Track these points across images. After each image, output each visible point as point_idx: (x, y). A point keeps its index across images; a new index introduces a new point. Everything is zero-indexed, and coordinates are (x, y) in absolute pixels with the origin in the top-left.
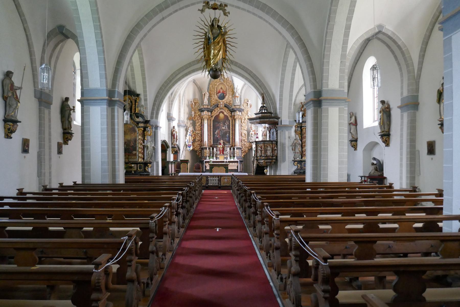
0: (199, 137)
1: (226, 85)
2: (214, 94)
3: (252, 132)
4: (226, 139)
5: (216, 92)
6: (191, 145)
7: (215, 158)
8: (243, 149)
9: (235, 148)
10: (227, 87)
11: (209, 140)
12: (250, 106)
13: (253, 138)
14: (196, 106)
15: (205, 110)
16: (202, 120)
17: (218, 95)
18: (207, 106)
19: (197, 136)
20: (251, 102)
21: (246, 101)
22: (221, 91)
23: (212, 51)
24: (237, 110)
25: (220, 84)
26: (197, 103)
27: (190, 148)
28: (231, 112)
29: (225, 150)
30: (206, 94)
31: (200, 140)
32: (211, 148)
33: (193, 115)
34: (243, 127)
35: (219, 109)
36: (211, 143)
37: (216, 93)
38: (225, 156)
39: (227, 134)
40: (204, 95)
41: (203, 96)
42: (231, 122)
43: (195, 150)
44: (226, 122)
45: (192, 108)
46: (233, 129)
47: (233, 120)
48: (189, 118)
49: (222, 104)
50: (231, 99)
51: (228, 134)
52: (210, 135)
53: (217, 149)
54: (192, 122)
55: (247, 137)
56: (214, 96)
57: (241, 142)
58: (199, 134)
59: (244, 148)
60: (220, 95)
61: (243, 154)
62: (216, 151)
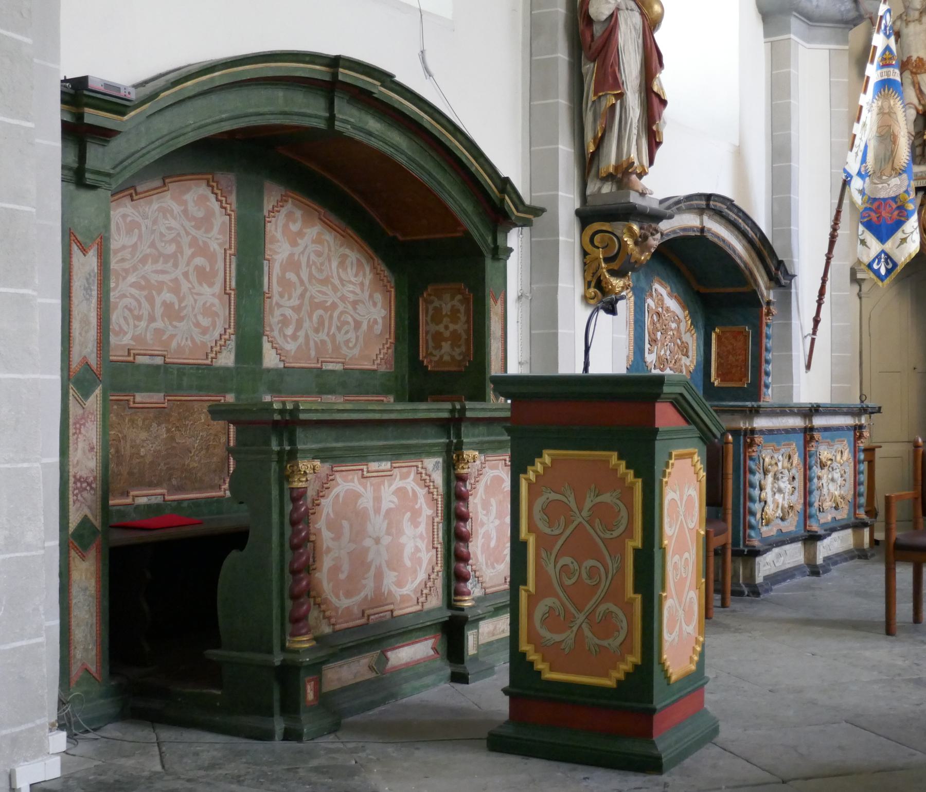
6: (902, 208)
27: (889, 246)
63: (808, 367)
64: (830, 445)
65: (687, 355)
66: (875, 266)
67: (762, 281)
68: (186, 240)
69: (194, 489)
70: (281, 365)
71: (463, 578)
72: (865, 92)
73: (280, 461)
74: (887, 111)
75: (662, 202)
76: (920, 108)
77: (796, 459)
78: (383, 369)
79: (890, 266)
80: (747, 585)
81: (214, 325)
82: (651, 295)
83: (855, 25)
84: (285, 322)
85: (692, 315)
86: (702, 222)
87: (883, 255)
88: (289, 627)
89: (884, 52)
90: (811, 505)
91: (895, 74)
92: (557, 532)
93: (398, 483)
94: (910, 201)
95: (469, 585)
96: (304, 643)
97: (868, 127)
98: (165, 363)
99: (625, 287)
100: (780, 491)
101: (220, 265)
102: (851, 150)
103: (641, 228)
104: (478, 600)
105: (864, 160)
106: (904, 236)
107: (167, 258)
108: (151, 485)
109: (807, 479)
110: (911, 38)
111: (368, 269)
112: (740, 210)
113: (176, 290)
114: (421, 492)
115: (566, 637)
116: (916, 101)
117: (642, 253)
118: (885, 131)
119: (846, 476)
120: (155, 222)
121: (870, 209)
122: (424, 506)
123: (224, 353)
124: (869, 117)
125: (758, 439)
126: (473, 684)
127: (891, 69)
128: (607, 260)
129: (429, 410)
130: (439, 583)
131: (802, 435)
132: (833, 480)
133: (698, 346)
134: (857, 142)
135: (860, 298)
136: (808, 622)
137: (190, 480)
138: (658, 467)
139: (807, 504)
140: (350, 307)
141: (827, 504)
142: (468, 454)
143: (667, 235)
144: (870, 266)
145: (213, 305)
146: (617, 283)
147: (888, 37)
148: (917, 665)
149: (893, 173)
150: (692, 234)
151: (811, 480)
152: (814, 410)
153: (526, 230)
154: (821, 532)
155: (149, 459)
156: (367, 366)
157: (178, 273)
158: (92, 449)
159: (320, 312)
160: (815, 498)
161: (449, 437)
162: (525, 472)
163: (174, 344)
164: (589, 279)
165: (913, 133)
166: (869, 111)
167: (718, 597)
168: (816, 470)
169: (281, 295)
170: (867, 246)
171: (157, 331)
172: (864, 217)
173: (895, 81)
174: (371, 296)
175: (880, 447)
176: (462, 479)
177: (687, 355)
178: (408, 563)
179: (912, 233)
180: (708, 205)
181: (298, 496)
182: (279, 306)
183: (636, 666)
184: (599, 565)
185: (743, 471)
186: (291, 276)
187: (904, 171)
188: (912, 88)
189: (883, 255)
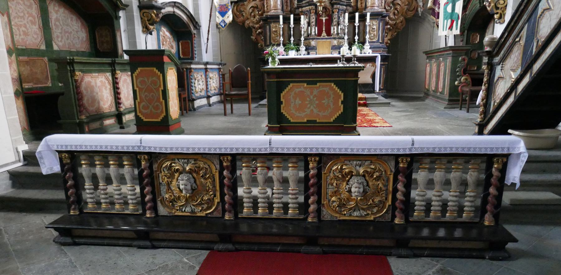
7: (304, 48)
8: (390, 18)
9: (368, 14)
32: (292, 16)
38: (335, 42)
59: (392, 16)
62: (306, 25)
63: (206, 52)
64: (212, 73)
65: (173, 48)
66: (221, 24)
67: (192, 28)
68: (26, 12)
69: (41, 84)
70: (59, 49)
71: (120, 104)
73: (71, 73)
75: (162, 3)
77: (203, 76)
78: (88, 51)
79: (225, 24)
80: (192, 108)
81: (38, 37)
82: (161, 31)
84: (58, 37)
85: (173, 37)
86: (174, 10)
88: (79, 114)
90: (208, 88)
92: (143, 87)
93: (100, 79)
95: (122, 105)
96: (83, 117)
98: (26, 48)
99: (154, 28)
100: (199, 84)
101: (37, 20)
103: (156, 12)
104: (125, 110)
107: (22, 17)
108: (28, 82)
109: (207, 82)
111: (79, 21)
112: (184, 6)
113: (25, 27)
114: (107, 82)
115: (148, 111)
117: (157, 19)
119: (217, 81)
120: (16, 6)
122: (108, 86)
123: (42, 45)
125: (193, 70)
126: (127, 129)
128: (148, 20)
129: (106, 60)
130: (114, 105)
131: (204, 70)
132: (213, 82)
133: (176, 46)
135: (219, 33)
136: (207, 115)
137: (38, 81)
138: (165, 71)
139: (207, 88)
140: (76, 32)
141: (213, 89)
142: (118, 72)
143: (164, 13)
144: (220, 24)
145: (36, 31)
146: (151, 27)
150: (171, 13)
151: (207, 82)
152: (207, 63)
153: (124, 11)
154: (211, 95)
155: (26, 75)
156: (83, 50)
157: (25, 22)
158: (15, 71)
159: (68, 34)
160: (209, 86)
161: (112, 67)
162: (134, 73)
163: (28, 43)
164: (143, 26)
167: (185, 111)
168: (209, 80)
169: (56, 29)
171: (22, 39)
174: (81, 30)
176: (117, 78)
177: (173, 48)
178: (106, 100)
180: (175, 5)
181: (76, 81)
182: (56, 32)
183: (164, 116)
184: (154, 94)
185: (189, 79)
186: (57, 23)
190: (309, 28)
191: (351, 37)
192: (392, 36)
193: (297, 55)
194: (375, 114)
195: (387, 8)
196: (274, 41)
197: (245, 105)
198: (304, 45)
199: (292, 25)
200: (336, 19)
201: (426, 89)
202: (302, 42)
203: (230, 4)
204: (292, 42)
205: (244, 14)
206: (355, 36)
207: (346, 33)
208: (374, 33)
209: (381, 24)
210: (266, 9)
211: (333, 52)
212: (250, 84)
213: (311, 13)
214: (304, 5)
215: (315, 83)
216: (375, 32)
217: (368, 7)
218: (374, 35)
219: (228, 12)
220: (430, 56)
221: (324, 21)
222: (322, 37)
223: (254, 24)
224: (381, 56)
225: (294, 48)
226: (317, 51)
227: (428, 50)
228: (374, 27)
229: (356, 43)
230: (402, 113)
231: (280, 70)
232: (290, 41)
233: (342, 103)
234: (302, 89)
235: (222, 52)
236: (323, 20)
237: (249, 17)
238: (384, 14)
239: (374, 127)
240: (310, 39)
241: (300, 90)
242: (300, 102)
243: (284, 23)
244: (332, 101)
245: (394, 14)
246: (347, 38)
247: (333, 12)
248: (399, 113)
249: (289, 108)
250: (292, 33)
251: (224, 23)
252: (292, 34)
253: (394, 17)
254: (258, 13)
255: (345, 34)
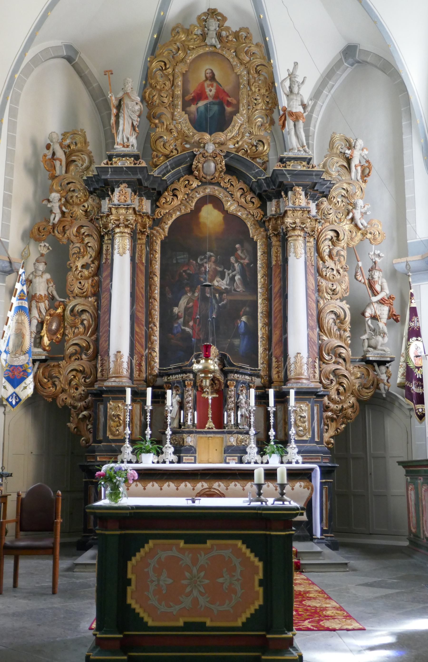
0: (81, 329)
1: (235, 62)
2: (173, 106)
3: (376, 305)
4: (237, 342)
5: (184, 96)
6: (25, 371)
7: (172, 449)
8: (330, 399)
9: (292, 393)
10: (240, 70)
11: (138, 347)
12: (359, 168)
13: (386, 339)
14: (72, 167)
15: (118, 183)
16: (102, 237)
17: (193, 108)
18: (128, 163)
19: (74, 326)
20: (366, 152)
21: (340, 145)
22: (207, 90)
23: (206, 482)
24: (298, 185)
25: (200, 56)
26: (79, 151)
27: (18, 390)
28: (260, 196)
29: (232, 405)
30: (127, 101)
31: (88, 348)
32: (149, 391)
33: (57, 210)
34: (325, 278)
35: (195, 185)
36: (149, 364)
37: (180, 103)
38: (233, 440)
39: (239, 317)
40: (119, 107)
41: (114, 111)
42: (259, 254)
43: (60, 403)
44: (233, 252)
45: (53, 177)
46: (276, 289)
47: (274, 240)
48: (36, 231)
49: (214, 156)
50: (262, 133)
51: (244, 319)
52: (149, 322)
53: (182, 396)
54: (51, 252)
55: (348, 334)
56: (169, 116)
57: (321, 358)
58: (85, 316)
59: (334, 395)
60: (202, 109)
61: (333, 426)
62: (176, 407)
66: (10, 400)
72: (10, 310)
74: (20, 322)
76: (40, 319)
83: (9, 274)
87: (14, 394)
89: (20, 293)
91: (26, 304)
94: (29, 368)
97: (11, 328)
102: (2, 339)
105: (7, 345)
106: (26, 385)
110: (37, 284)
116: (37, 316)
118: (19, 331)
121: (9, 371)
124: (12, 323)
127: (24, 301)
134: (5, 335)
135: (5, 414)
144: (7, 400)
147: (23, 285)
148: (9, 607)
149: (22, 353)
165: (35, 332)
166: (12, 320)
170: (6, 389)
172: (6, 374)
173: (25, 307)
175: (10, 495)
179: (29, 384)
187: (27, 353)
188: (36, 309)
189: (14, 394)
190: (182, 412)
191: (262, 430)
192: (336, 430)
193: (158, 462)
194: (323, 592)
195: (324, 381)
196: (113, 434)
197: (48, 559)
198: (171, 444)
199: (148, 407)
200: (233, 399)
201: (413, 533)
202: (169, 437)
203: (31, 365)
204: (148, 437)
205: (57, 383)
206: (269, 430)
207: (252, 423)
208: (304, 424)
209: (315, 408)
210: (99, 375)
211: (228, 458)
212: (59, 526)
213: (185, 386)
214: (173, 371)
215: (202, 540)
216: (306, 424)
217: (291, 379)
218: (304, 428)
219: (25, 378)
220: (411, 471)
221: (210, 401)
222: (206, 430)
223: (76, 400)
224: (320, 467)
225: (152, 448)
226: (197, 455)
227: (405, 459)
228: (303, 415)
229: (272, 443)
230: (375, 589)
231: (128, 511)
232: (144, 435)
233: (260, 585)
234: (174, 553)
235: (6, 450)
236: (207, 399)
237: (67, 387)
238: (322, 391)
239: (328, 629)
240: (183, 432)
241: (169, 553)
242: (170, 581)
243: (133, 400)
244: (238, 580)
245: (339, 393)
246: (254, 432)
247: (227, 386)
248: (371, 589)
249: (146, 593)
250: (148, 420)
251: (16, 399)
252: (148, 423)
253: (338, 397)
254: (85, 381)
255: (250, 427)
